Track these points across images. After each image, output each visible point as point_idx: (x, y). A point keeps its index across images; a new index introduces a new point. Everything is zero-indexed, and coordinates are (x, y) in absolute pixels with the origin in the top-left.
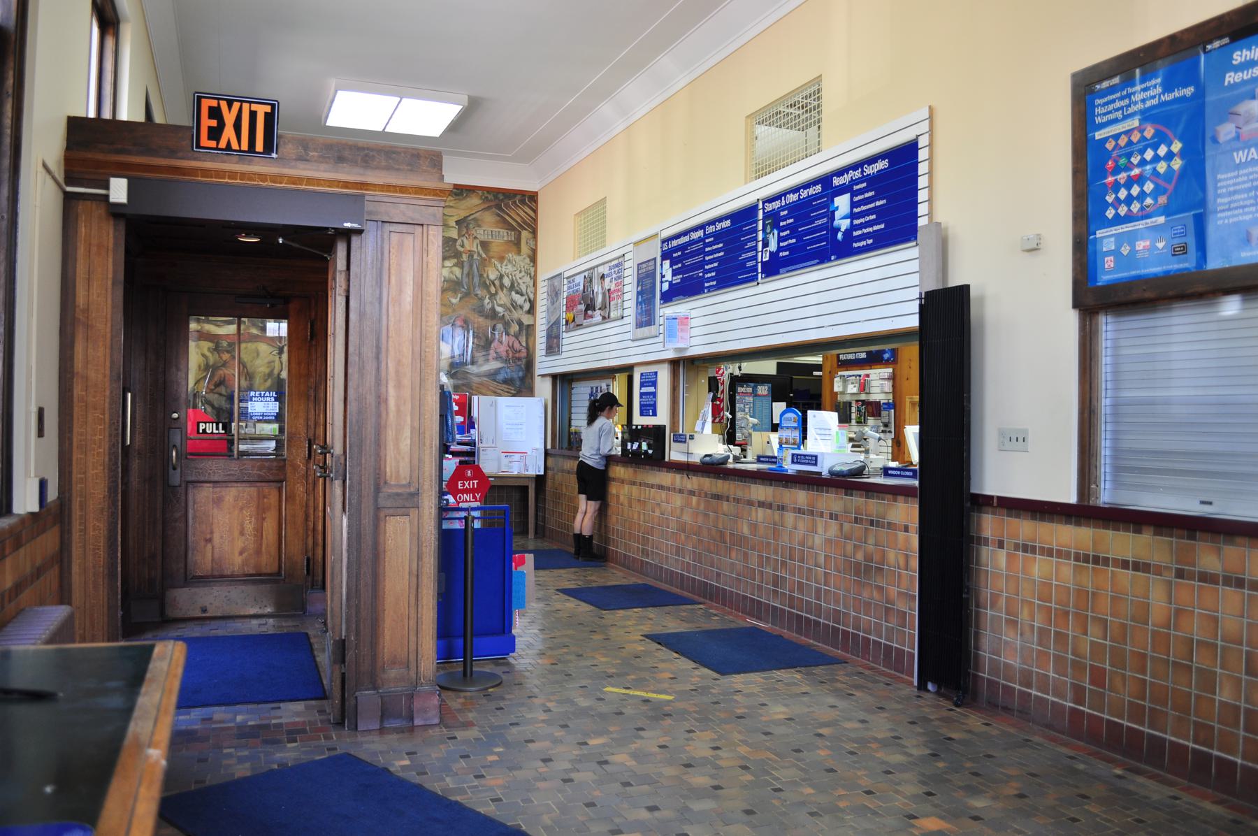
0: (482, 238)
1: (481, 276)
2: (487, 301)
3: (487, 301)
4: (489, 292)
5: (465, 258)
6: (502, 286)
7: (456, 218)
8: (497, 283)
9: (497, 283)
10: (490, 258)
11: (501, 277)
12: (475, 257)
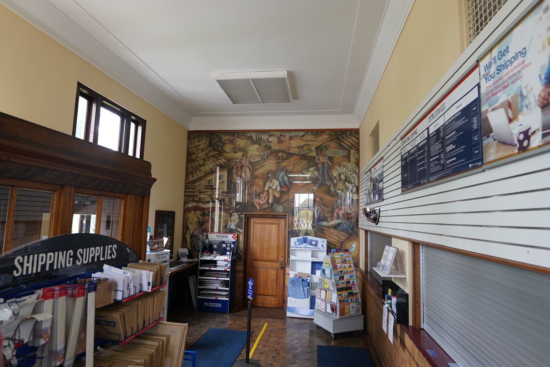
0: (329, 155)
1: (329, 175)
2: (332, 187)
3: (332, 187)
4: (333, 183)
5: (320, 166)
6: (340, 179)
7: (315, 146)
8: (337, 178)
9: (337, 178)
10: (334, 165)
11: (340, 175)
12: (326, 165)
